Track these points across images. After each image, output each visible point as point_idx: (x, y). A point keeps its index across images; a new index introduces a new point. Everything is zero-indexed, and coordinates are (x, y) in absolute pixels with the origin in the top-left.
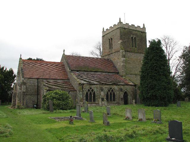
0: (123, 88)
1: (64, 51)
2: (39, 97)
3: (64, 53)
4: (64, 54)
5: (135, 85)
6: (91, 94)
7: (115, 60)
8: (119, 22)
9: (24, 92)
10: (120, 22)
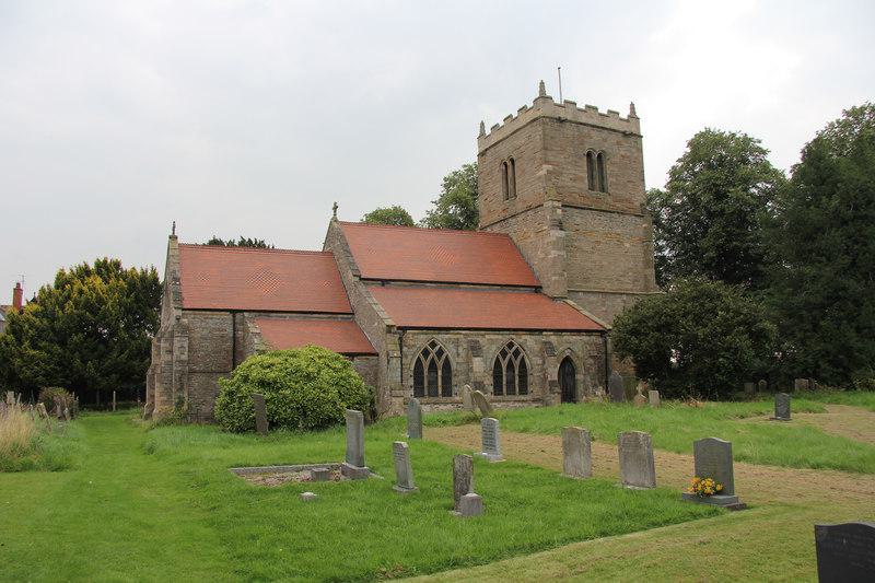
1: (335, 208)
5: (603, 333)
6: (433, 366)
10: (543, 97)
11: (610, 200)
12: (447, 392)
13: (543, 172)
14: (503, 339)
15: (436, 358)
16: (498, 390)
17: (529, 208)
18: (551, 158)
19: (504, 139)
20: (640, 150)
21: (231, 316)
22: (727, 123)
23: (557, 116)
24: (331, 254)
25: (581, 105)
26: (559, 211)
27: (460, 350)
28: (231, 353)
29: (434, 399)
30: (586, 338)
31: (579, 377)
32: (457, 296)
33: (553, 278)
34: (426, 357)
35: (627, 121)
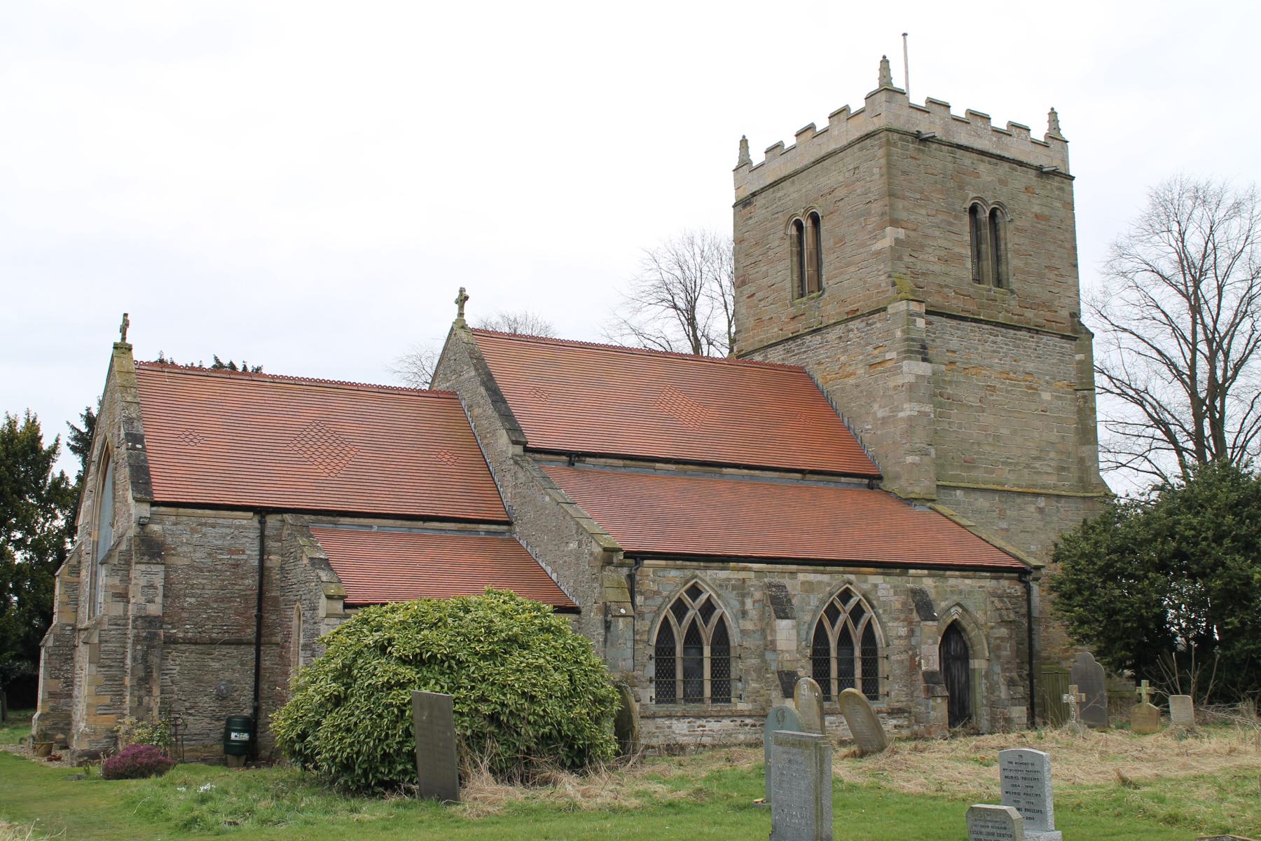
0: (932, 594)
1: (462, 299)
2: (266, 663)
3: (461, 314)
4: (464, 327)
5: (1023, 574)
6: (693, 637)
7: (851, 381)
8: (875, 86)
9: (150, 621)
10: (887, 90)
11: (1013, 303)
12: (722, 692)
13: (886, 243)
14: (829, 581)
15: (700, 621)
16: (665, 692)
17: (853, 316)
18: (903, 215)
19: (796, 173)
20: (1070, 206)
21: (256, 519)
22: (850, 106)
23: (914, 130)
24: (451, 396)
25: (958, 111)
26: (921, 323)
27: (749, 603)
28: (254, 602)
29: (693, 708)
30: (989, 584)
31: (978, 664)
32: (721, 489)
33: (909, 459)
34: (680, 618)
35: (1045, 145)
